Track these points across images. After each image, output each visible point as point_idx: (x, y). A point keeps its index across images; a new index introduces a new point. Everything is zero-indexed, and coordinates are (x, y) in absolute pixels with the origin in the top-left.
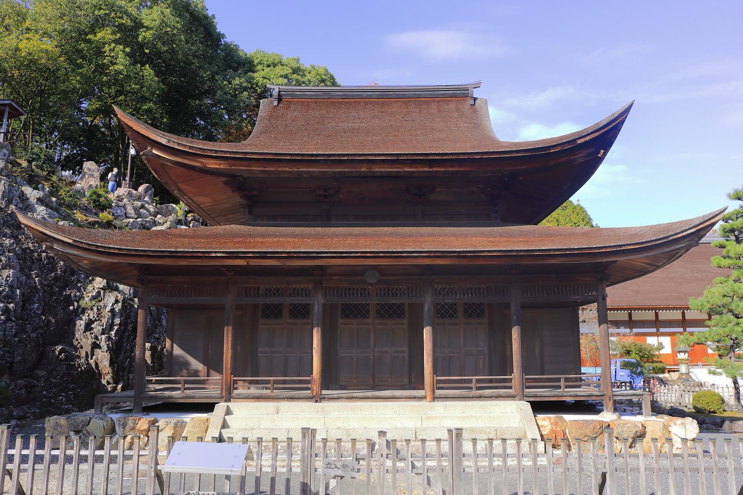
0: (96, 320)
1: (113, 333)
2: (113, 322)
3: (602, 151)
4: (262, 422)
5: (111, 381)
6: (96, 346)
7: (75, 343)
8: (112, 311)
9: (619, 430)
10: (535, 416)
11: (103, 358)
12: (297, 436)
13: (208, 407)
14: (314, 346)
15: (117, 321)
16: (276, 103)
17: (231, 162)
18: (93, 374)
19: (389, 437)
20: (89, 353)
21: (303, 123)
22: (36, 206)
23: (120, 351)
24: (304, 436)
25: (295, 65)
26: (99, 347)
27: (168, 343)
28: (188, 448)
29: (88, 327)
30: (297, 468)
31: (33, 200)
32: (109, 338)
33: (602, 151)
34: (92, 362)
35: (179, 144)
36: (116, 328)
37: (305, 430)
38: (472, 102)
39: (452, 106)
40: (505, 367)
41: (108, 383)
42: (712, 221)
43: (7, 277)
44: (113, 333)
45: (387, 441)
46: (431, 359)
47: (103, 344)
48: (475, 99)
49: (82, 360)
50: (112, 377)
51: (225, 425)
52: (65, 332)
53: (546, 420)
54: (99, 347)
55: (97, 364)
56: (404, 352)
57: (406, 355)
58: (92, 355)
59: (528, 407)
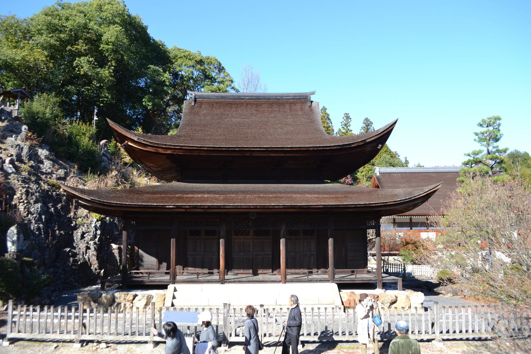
0: (87, 232)
1: (97, 239)
2: (96, 233)
3: (380, 145)
4: (202, 299)
5: (97, 268)
6: (88, 248)
7: (74, 245)
8: (95, 227)
9: (383, 299)
10: (340, 291)
11: (92, 256)
12: (221, 307)
13: (164, 287)
14: (221, 253)
15: (99, 232)
16: (193, 104)
17: (173, 150)
18: (86, 265)
19: (265, 307)
20: (84, 252)
21: (210, 118)
22: (44, 161)
23: (103, 250)
24: (225, 307)
25: (198, 58)
26: (90, 249)
27: (136, 248)
28: (137, 307)
29: (83, 237)
30: (221, 323)
31: (43, 157)
32: (95, 243)
33: (380, 145)
34: (86, 257)
35: (144, 141)
36: (98, 237)
37: (225, 305)
38: (309, 104)
39: (298, 106)
40: (326, 266)
41: (96, 270)
42: (435, 189)
43: (38, 208)
44: (97, 239)
45: (264, 310)
46: (284, 260)
47: (92, 247)
48: (312, 102)
49: (81, 257)
50: (98, 266)
51: (174, 297)
52: (70, 241)
53: (346, 293)
54: (90, 249)
55: (89, 259)
56: (269, 255)
57: (270, 256)
58: (86, 253)
59: (336, 286)
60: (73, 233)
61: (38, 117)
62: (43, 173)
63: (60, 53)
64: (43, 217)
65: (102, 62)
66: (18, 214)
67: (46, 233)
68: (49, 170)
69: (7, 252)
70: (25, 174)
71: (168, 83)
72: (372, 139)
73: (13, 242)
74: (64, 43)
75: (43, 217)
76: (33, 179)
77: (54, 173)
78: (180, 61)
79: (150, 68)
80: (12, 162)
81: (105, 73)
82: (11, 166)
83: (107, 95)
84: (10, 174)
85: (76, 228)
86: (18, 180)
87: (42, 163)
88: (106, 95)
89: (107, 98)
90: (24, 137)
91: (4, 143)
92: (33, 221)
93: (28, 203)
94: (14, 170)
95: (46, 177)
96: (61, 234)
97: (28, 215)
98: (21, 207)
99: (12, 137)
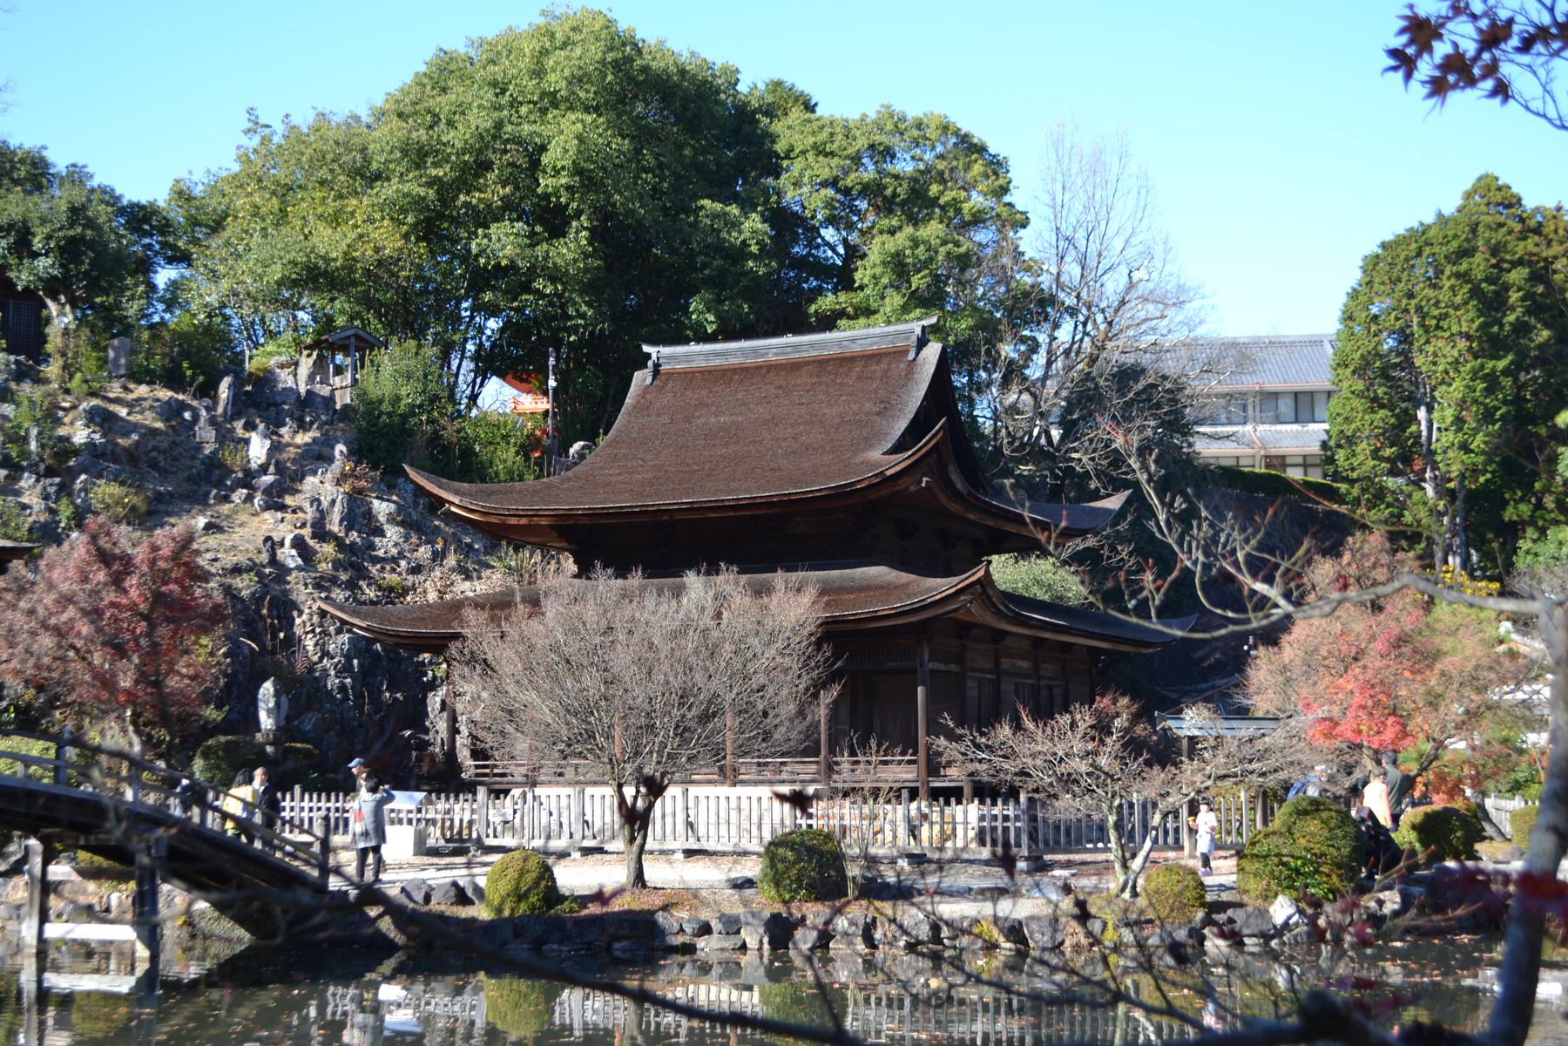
22: (385, 527)
31: (382, 519)
52: (417, 716)
60: (425, 697)
61: (381, 413)
62: (376, 560)
63: (435, 224)
64: (355, 662)
65: (552, 220)
66: (299, 656)
67: (359, 697)
68: (394, 551)
69: (259, 730)
70: (326, 567)
71: (754, 249)
72: (898, 468)
73: (269, 711)
74: (446, 190)
75: (355, 662)
76: (344, 577)
77: (405, 557)
78: (797, 166)
79: (702, 207)
80: (299, 543)
81: (570, 250)
82: (294, 552)
83: (584, 308)
84: (289, 571)
85: (432, 686)
86: (306, 585)
87: (382, 533)
88: (582, 309)
89: (583, 316)
90: (338, 471)
91: (298, 491)
92: (333, 673)
93: (325, 633)
94: (300, 561)
95: (383, 568)
96: (396, 699)
97: (321, 659)
98: (309, 643)
99: (315, 473)
